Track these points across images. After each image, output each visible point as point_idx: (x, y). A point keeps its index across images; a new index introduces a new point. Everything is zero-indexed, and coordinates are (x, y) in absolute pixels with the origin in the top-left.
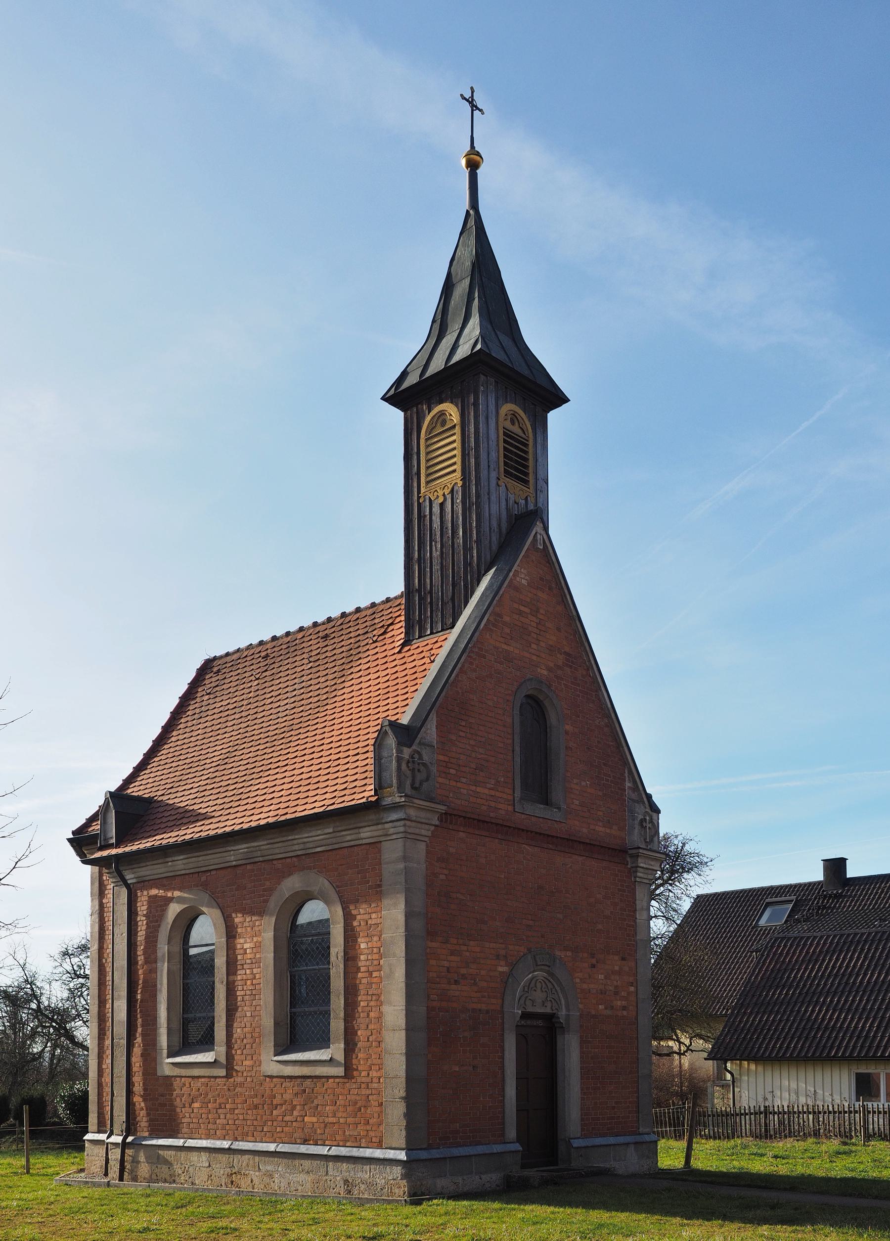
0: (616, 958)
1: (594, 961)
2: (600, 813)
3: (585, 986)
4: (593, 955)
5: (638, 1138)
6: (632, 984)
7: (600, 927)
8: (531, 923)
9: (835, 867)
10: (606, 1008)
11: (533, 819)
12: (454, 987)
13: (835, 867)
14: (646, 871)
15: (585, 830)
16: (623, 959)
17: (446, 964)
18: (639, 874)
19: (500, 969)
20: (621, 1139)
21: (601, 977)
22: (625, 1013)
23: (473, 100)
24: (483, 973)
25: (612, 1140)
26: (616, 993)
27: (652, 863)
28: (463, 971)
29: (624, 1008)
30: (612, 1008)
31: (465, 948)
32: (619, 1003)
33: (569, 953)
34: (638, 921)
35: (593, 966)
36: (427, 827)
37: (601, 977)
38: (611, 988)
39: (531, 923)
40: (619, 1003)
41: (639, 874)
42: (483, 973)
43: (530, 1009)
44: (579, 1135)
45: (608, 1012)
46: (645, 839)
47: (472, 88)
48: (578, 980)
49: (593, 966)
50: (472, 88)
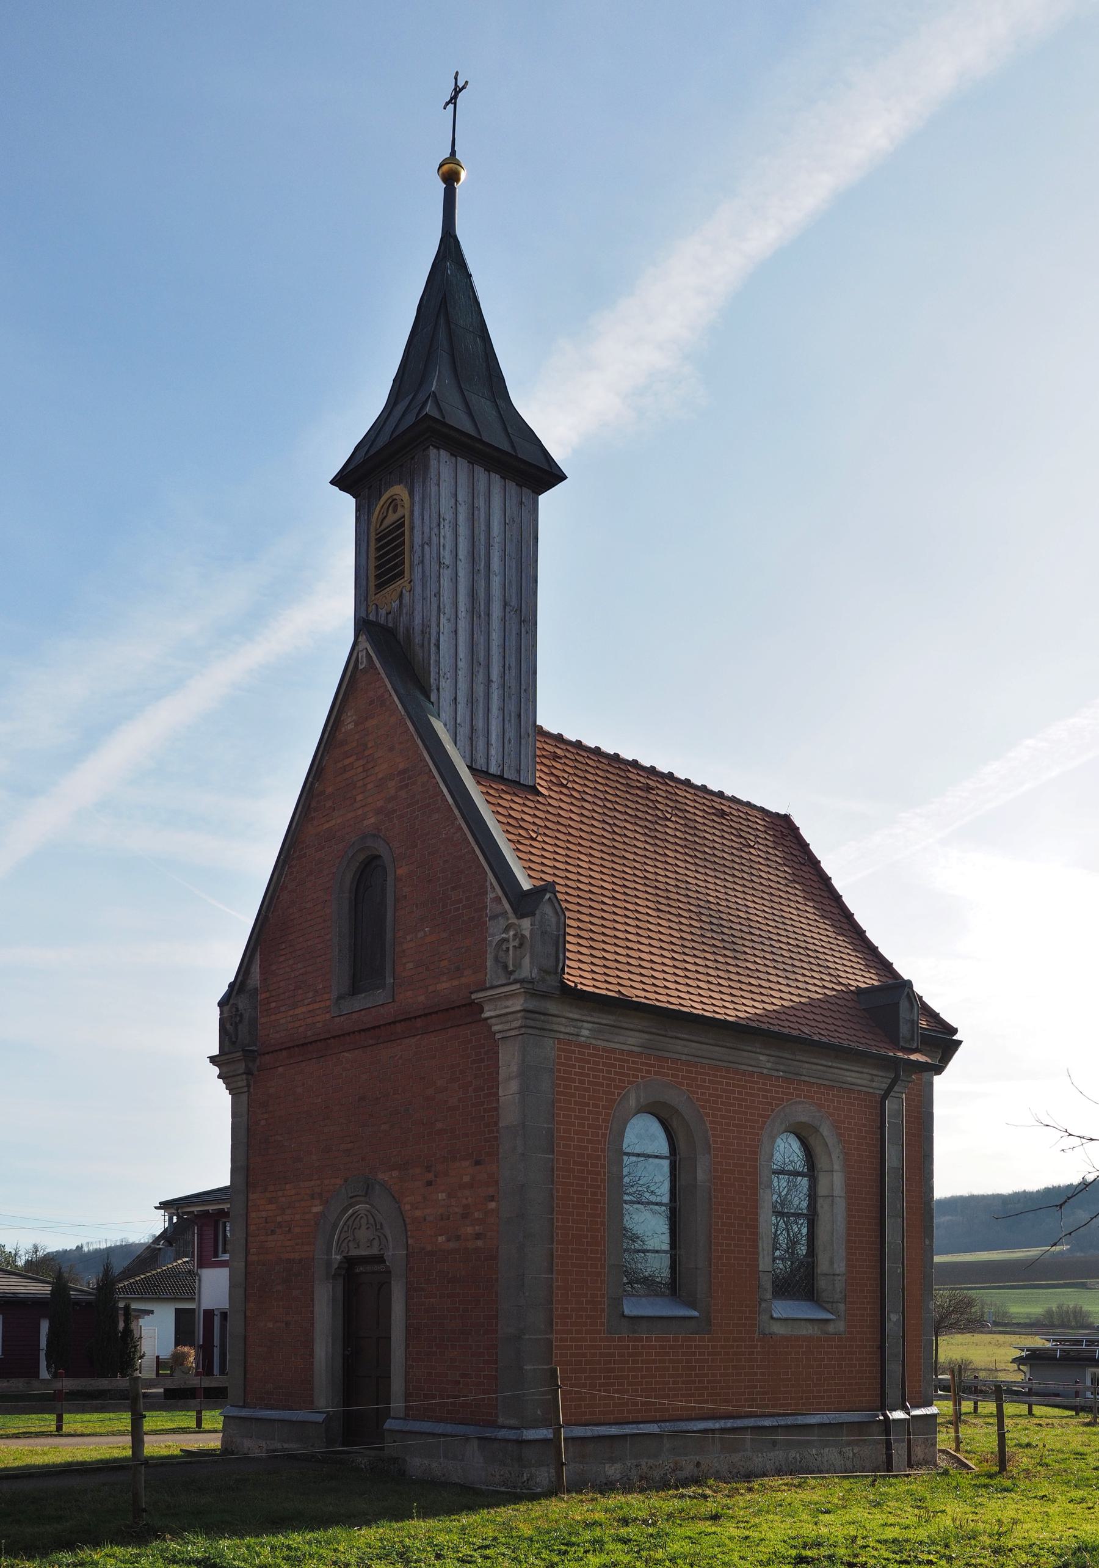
0: (466, 1164)
1: (430, 1176)
2: (445, 963)
3: (418, 1213)
4: (428, 1169)
5: (488, 1433)
6: (492, 1198)
7: (439, 1126)
8: (350, 1146)
9: (213, 1060)
10: (448, 1240)
11: (355, 1016)
12: (270, 1238)
13: (213, 1060)
14: (504, 1019)
15: (422, 998)
16: (477, 1163)
17: (264, 1214)
18: (495, 1028)
19: (315, 1210)
20: (460, 1429)
21: (441, 1196)
22: (480, 1243)
23: (452, 99)
24: (298, 1217)
25: (449, 1428)
26: (465, 1216)
27: (509, 1003)
28: (279, 1219)
29: (478, 1236)
30: (458, 1238)
31: (280, 1193)
32: (469, 1230)
33: (395, 1173)
34: (501, 1100)
35: (429, 1183)
36: (239, 1078)
37: (441, 1196)
38: (456, 1210)
39: (350, 1146)
40: (469, 1230)
41: (495, 1028)
42: (298, 1217)
43: (354, 1253)
44: (402, 1415)
45: (452, 1245)
46: (506, 967)
47: (467, 82)
48: (408, 1207)
49: (429, 1183)
50: (467, 82)
